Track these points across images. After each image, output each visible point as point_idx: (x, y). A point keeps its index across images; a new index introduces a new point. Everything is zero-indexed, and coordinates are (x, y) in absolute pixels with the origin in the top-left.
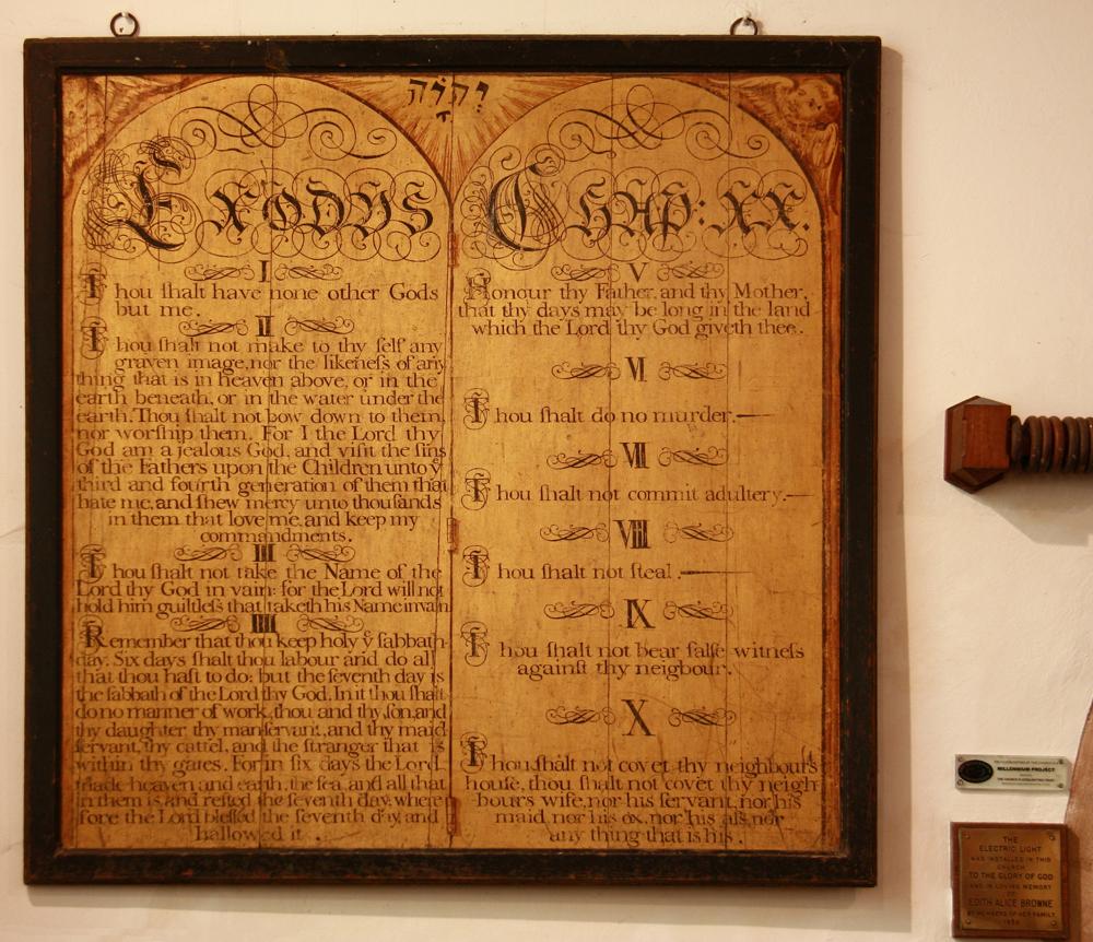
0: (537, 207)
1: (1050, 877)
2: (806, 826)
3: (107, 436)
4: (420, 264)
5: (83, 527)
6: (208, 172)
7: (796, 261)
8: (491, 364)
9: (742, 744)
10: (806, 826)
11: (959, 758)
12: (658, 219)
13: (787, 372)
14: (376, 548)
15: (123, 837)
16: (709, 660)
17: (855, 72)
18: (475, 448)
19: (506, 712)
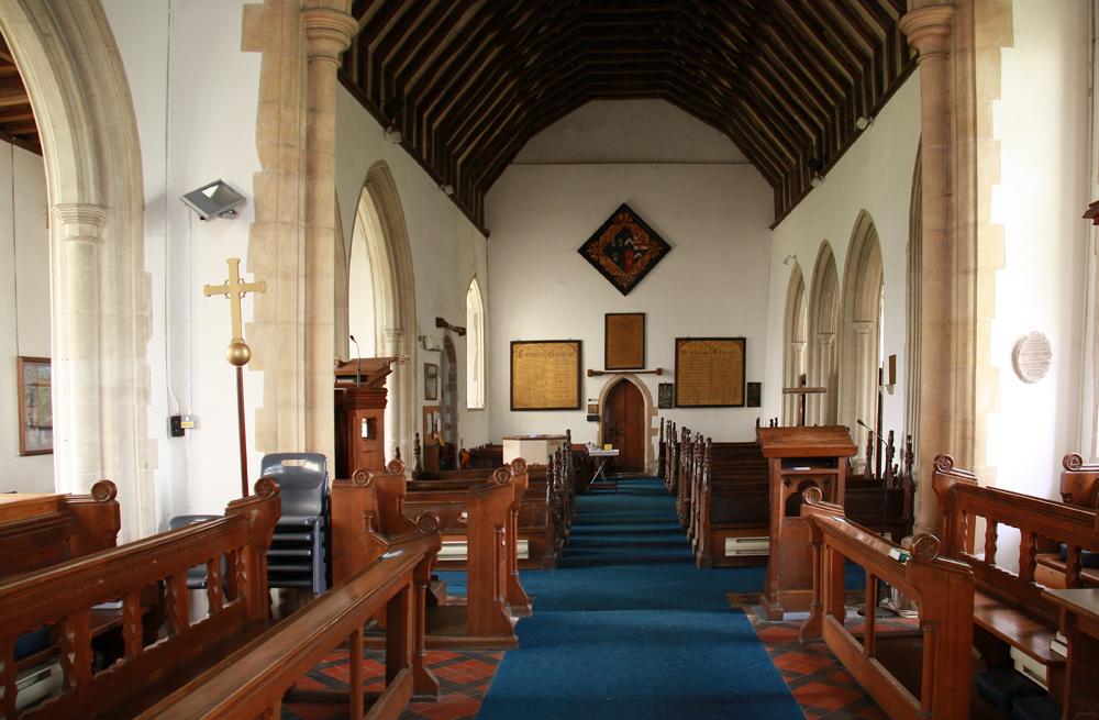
0: (960, 275)
1: (367, 644)
2: (575, 405)
3: (516, 374)
4: (542, 359)
5: (515, 381)
6: (525, 352)
7: (574, 358)
8: (549, 367)
9: (570, 398)
10: (575, 405)
11: (1012, 46)
12: (564, 355)
13: (574, 368)
14: (539, 383)
15: (519, 407)
16: (567, 392)
17: (579, 343)
18: (548, 374)
19: (549, 396)
